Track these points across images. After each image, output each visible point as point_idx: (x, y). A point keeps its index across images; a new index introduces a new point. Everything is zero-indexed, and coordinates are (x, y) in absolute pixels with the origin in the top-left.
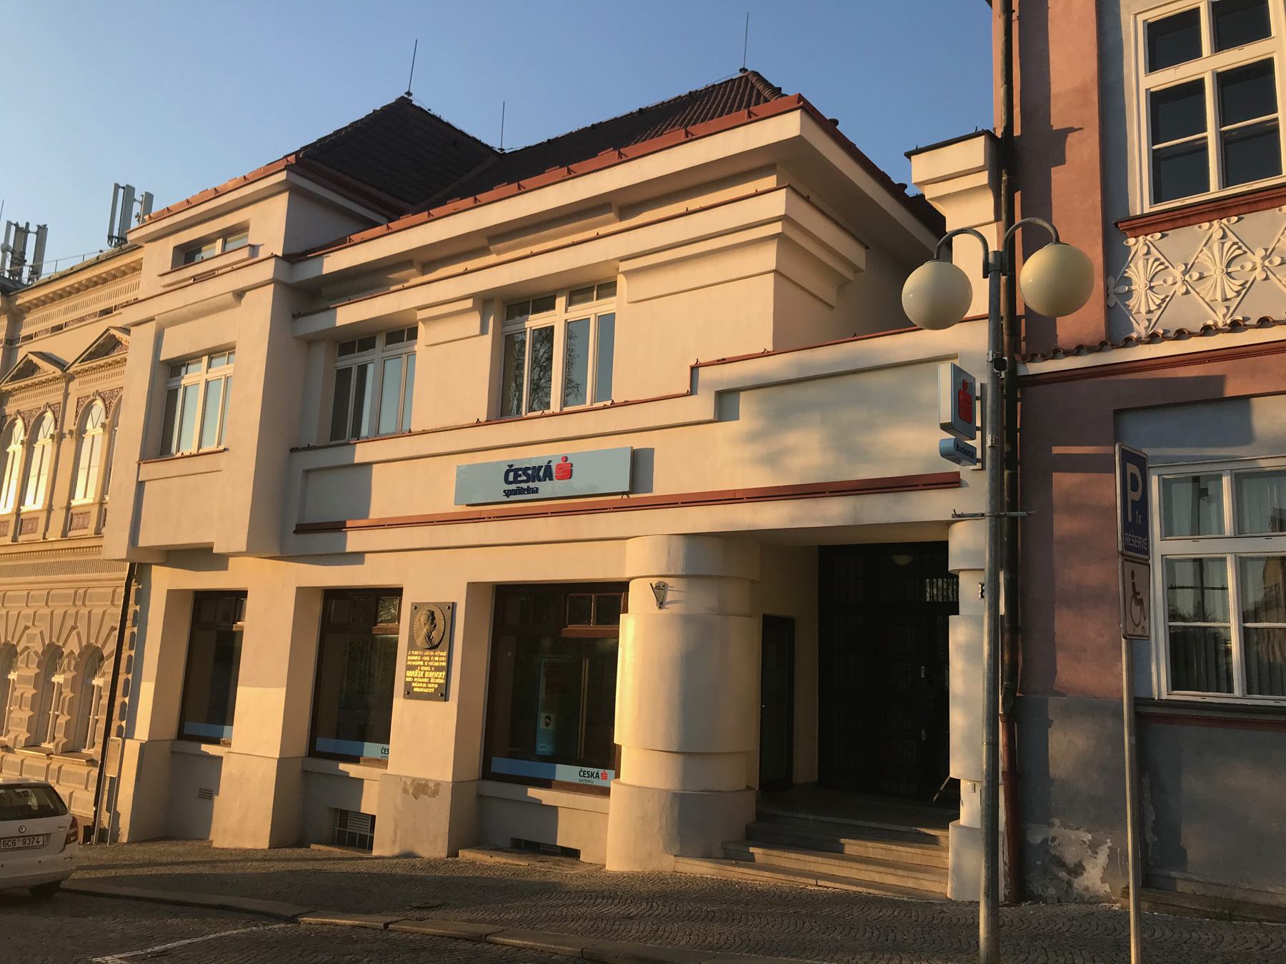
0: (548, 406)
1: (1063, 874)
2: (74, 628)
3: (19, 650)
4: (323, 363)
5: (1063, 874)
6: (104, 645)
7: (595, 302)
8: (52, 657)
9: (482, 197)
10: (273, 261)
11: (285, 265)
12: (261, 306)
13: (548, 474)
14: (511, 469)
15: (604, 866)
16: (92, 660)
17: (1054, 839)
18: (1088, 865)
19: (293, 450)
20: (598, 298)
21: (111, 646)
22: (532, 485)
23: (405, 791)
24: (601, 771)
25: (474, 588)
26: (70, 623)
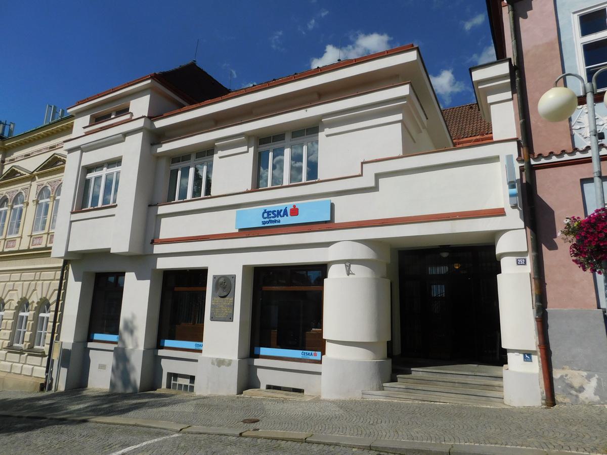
0: (301, 180)
1: (573, 392)
2: (35, 290)
3: (5, 301)
4: (164, 168)
5: (573, 392)
6: (5, 297)
7: (272, 143)
8: (24, 304)
9: (202, 104)
10: (143, 119)
11: (149, 121)
12: (135, 143)
13: (285, 213)
14: (265, 211)
15: (320, 396)
16: (44, 304)
17: (566, 375)
18: (586, 387)
19: (150, 206)
20: (273, 142)
21: (54, 298)
22: (276, 219)
23: (213, 363)
24: (313, 352)
25: (245, 268)
26: (32, 288)
